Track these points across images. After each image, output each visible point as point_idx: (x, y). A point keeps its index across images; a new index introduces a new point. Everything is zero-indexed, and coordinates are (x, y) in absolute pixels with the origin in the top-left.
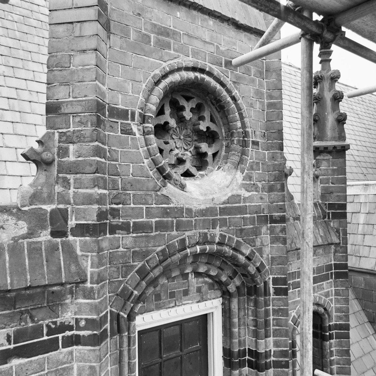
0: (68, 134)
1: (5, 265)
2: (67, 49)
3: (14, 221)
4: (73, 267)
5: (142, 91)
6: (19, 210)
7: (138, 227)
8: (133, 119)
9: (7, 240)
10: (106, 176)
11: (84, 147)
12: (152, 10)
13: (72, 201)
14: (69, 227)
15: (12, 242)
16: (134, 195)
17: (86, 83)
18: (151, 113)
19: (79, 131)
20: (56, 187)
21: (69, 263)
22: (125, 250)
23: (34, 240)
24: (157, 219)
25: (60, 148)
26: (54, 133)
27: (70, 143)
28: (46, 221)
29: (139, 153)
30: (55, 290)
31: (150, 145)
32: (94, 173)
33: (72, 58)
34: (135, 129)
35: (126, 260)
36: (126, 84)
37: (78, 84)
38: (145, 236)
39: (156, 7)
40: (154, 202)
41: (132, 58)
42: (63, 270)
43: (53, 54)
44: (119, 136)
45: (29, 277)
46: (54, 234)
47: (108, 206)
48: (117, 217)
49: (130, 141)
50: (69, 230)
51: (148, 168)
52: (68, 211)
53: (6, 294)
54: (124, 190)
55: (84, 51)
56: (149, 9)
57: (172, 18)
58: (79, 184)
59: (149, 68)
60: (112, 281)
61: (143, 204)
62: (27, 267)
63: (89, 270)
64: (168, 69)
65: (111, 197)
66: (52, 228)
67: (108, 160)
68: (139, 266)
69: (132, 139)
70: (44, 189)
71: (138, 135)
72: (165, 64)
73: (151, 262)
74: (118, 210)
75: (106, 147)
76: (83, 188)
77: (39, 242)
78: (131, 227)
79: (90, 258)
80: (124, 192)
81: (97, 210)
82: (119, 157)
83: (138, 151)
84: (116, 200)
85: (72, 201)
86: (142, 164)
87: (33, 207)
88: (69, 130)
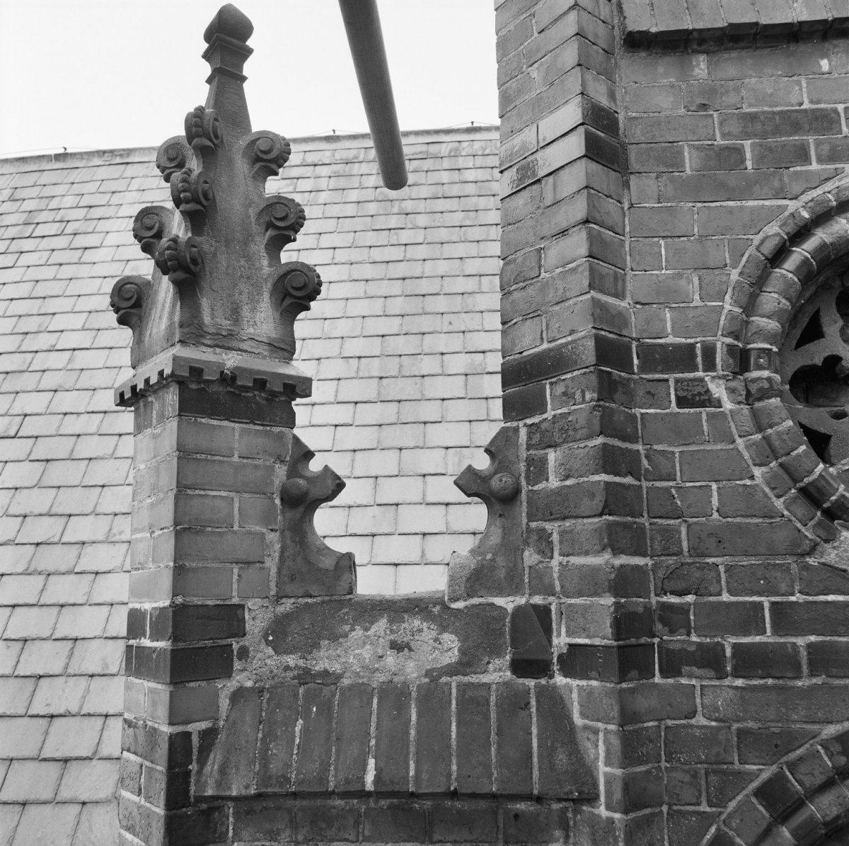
0: (544, 426)
1: (408, 733)
2: (532, 239)
3: (434, 634)
4: (561, 757)
5: (730, 290)
6: (446, 608)
7: (749, 662)
8: (710, 365)
9: (415, 675)
10: (644, 520)
11: (577, 452)
12: (739, 83)
13: (558, 588)
14: (556, 653)
15: (427, 680)
16: (729, 569)
17: (571, 302)
18: (766, 340)
19: (563, 415)
20: (526, 553)
21: (552, 746)
22: (713, 724)
23: (474, 679)
24: (813, 638)
25: (530, 461)
26: (516, 430)
27: (550, 446)
28: (502, 634)
29: (735, 453)
30: (523, 812)
31: (771, 426)
32: (601, 515)
33: (543, 256)
34: (718, 390)
35: (718, 754)
36: (683, 282)
37: (557, 308)
38: (774, 687)
39: (751, 72)
40: (797, 588)
41: (692, 216)
42: (535, 760)
43: (510, 258)
44: (671, 414)
45: (454, 767)
46: (521, 667)
47: (654, 600)
48: (683, 631)
49: (705, 424)
50: (555, 660)
51: (767, 490)
52: (550, 611)
53: (412, 803)
54: (698, 556)
55: (564, 232)
56: (731, 83)
57: (804, 85)
58: (572, 545)
59: (744, 226)
60: (679, 812)
61: (760, 594)
62: (454, 743)
63: (603, 770)
64: (806, 215)
65: (660, 574)
66: (514, 654)
67: (647, 480)
68: (765, 776)
69: (711, 417)
70: (498, 559)
71: (728, 405)
72: (792, 205)
73: (803, 768)
74: (683, 610)
75: (640, 447)
76: (578, 554)
77: (485, 684)
78: (729, 660)
79: (601, 735)
80: (697, 560)
81: (612, 609)
82: (678, 468)
83: (732, 447)
84: (674, 581)
85: (558, 588)
86: (748, 482)
87: (476, 601)
88: (545, 416)
